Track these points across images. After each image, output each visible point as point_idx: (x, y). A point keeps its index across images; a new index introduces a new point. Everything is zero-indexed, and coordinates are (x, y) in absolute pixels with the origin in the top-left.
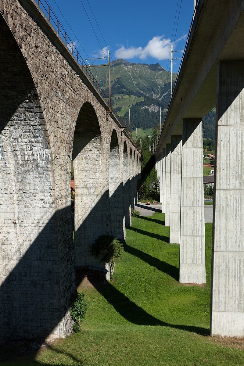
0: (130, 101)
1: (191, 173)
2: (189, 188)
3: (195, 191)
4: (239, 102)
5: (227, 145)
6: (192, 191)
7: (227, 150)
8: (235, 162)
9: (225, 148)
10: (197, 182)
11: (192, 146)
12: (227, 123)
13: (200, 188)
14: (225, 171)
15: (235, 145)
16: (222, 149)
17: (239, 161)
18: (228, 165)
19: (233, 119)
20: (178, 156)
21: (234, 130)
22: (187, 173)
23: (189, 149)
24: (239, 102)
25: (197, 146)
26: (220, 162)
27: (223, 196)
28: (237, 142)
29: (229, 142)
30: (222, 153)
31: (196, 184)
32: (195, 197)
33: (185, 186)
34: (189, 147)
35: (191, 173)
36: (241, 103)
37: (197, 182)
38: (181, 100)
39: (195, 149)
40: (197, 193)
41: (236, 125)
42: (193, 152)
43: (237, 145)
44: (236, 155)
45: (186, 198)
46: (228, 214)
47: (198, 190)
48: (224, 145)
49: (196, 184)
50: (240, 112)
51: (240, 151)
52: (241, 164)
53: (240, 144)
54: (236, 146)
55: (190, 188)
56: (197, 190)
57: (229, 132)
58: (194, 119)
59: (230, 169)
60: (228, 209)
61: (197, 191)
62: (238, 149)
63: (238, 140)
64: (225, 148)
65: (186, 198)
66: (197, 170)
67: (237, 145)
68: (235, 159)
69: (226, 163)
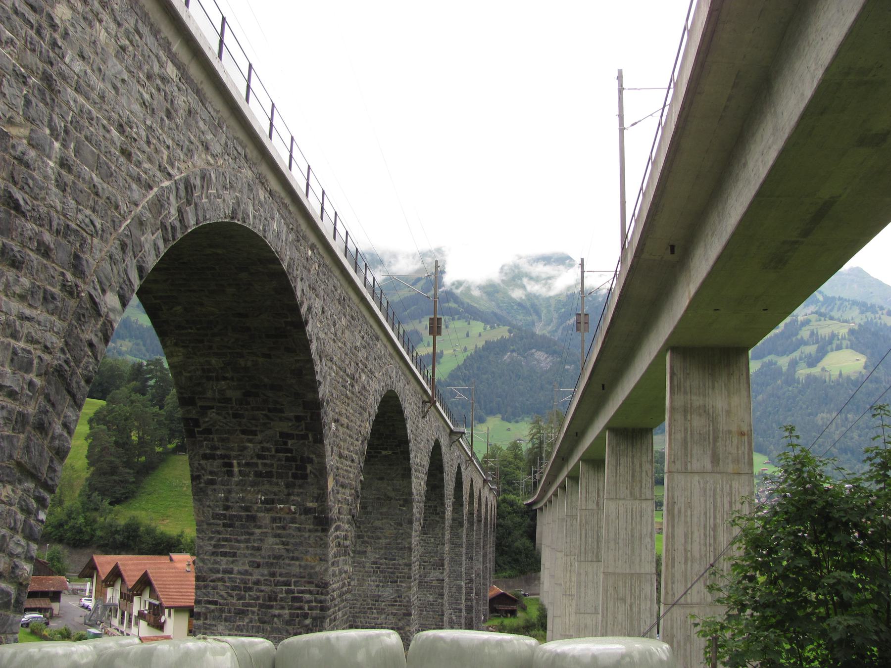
0: (468, 335)
1: (626, 562)
2: (622, 599)
3: (635, 609)
4: (709, 427)
5: (686, 511)
6: (628, 606)
7: (686, 522)
8: (702, 547)
9: (683, 518)
10: (640, 586)
11: (629, 496)
12: (686, 469)
13: (649, 602)
14: (683, 566)
15: (703, 512)
16: (676, 520)
17: (710, 545)
18: (689, 554)
19: (698, 460)
20: (598, 513)
21: (699, 482)
22: (615, 561)
23: (623, 501)
24: (709, 427)
25: (641, 496)
26: (672, 546)
27: (679, 618)
28: (706, 507)
29: (689, 505)
30: (676, 529)
31: (637, 590)
32: (635, 623)
33: (611, 594)
34: (622, 496)
35: (626, 562)
36: (711, 428)
37: (640, 586)
38: (603, 389)
39: (637, 502)
40: (639, 613)
41: (702, 473)
42: (632, 511)
43: (705, 513)
44: (705, 534)
45: (614, 625)
46: (689, 658)
47: (643, 607)
48: (680, 512)
49: (637, 590)
50: (711, 446)
51: (712, 526)
52: (714, 552)
53: (712, 510)
54: (309, 590)
55: (624, 600)
56: (640, 605)
57: (689, 485)
58: (634, 430)
59: (692, 562)
60: (688, 645)
61: (640, 609)
62: (708, 520)
63: (708, 503)
64: (683, 518)
65: (614, 625)
66: (640, 556)
67: (705, 513)
68: (702, 542)
69: (685, 550)
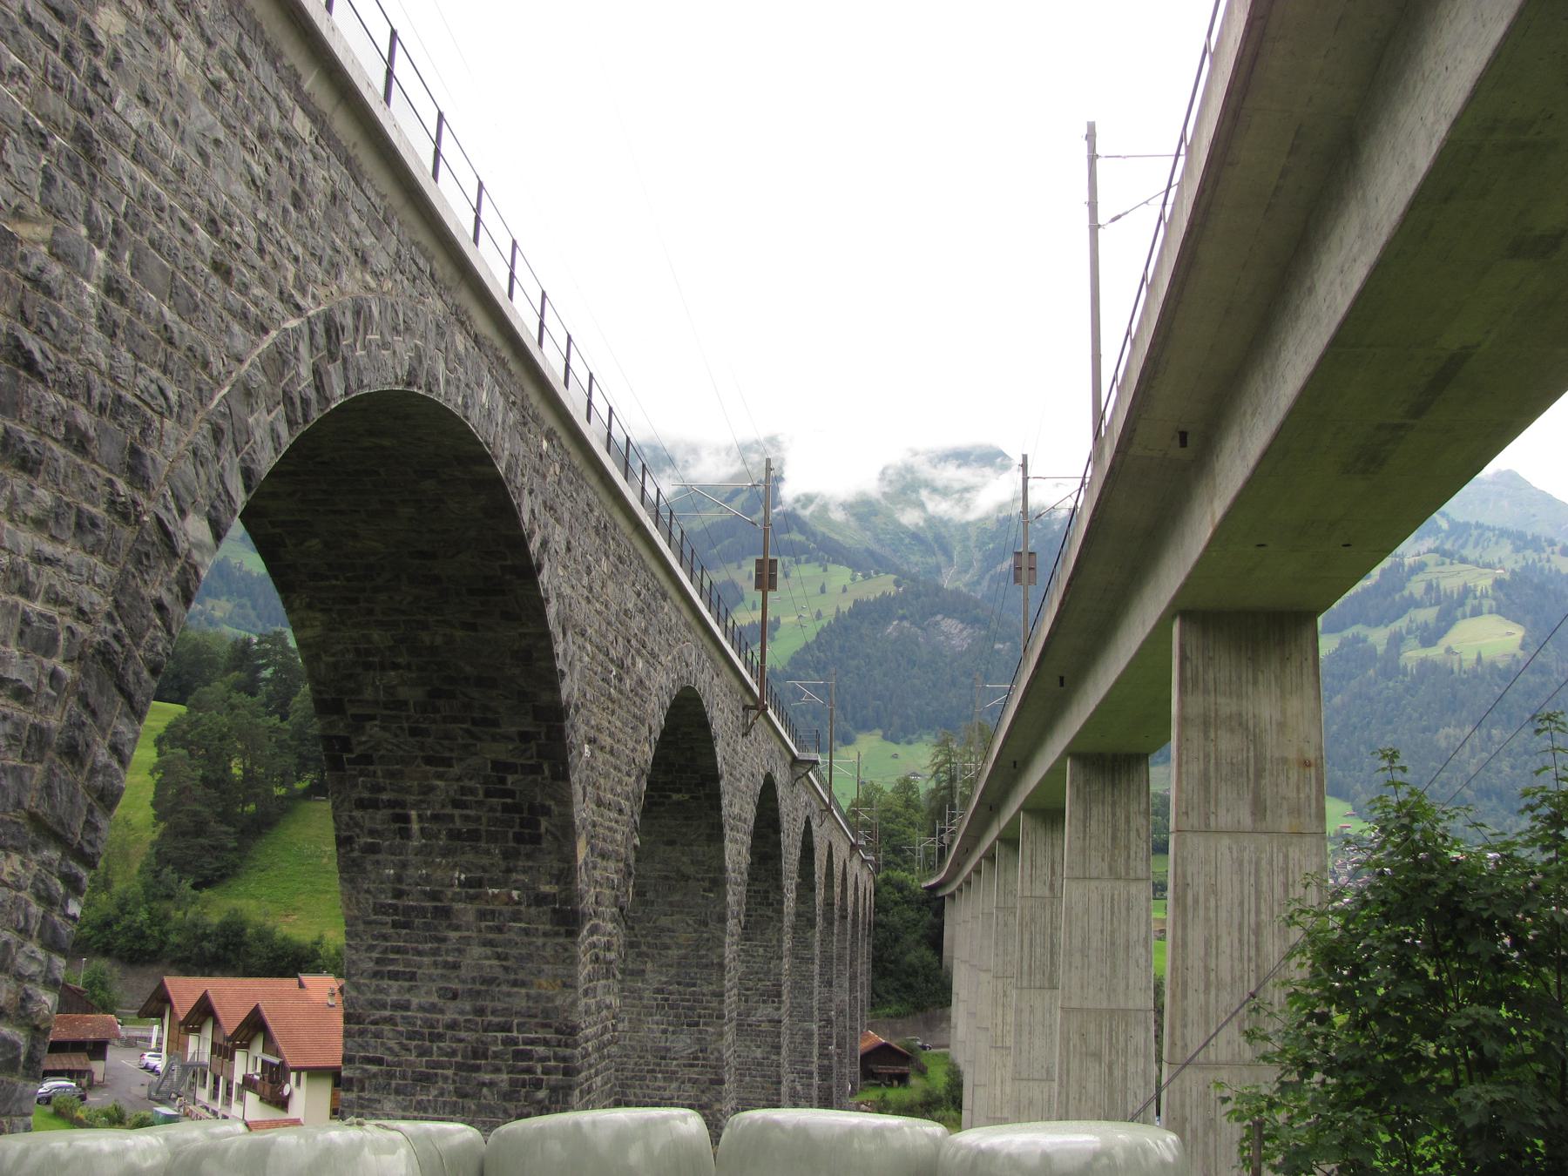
0: (823, 591)
1: (1101, 989)
2: (1094, 1055)
3: (1118, 1073)
4: (1248, 751)
5: (1207, 900)
6: (1104, 1068)
7: (1207, 920)
8: (1236, 963)
9: (1201, 912)
10: (1126, 1031)
11: (1107, 873)
12: (1207, 825)
13: (1141, 1060)
14: (1202, 996)
15: (1236, 902)
16: (1190, 916)
17: (1250, 959)
18: (1213, 976)
19: (1228, 810)
20: (1052, 904)
21: (1230, 849)
22: (1082, 987)
23: (1096, 883)
24: (1248, 751)
25: (1127, 873)
26: (1183, 961)
27: (1194, 1089)
28: (1242, 892)
29: (1213, 890)
30: (1189, 930)
31: (1121, 1039)
32: (1118, 1097)
33: (1074, 1046)
34: (1094, 873)
35: (1101, 989)
36: (1252, 754)
37: (1126, 1031)
38: (1062, 684)
39: (1121, 884)
40: (1125, 1079)
41: (1235, 832)
42: (1113, 899)
43: (1241, 904)
44: (1240, 941)
45: (1080, 1100)
46: (1212, 1158)
47: (1131, 1068)
48: (1196, 901)
49: (1121, 1039)
50: (1251, 785)
51: (1253, 925)
52: (1257, 973)
53: (1253, 899)
54: (545, 1039)
55: (1097, 1056)
56: (1126, 1065)
57: (1213, 854)
58: (1115, 757)
59: (1218, 989)
60: (1211, 1135)
61: (1126, 1071)
62: (1246, 916)
63: (1246, 885)
64: (1201, 912)
65: (1080, 1100)
66: (1127, 979)
67: (1241, 904)
68: (1236, 954)
69: (1206, 968)
